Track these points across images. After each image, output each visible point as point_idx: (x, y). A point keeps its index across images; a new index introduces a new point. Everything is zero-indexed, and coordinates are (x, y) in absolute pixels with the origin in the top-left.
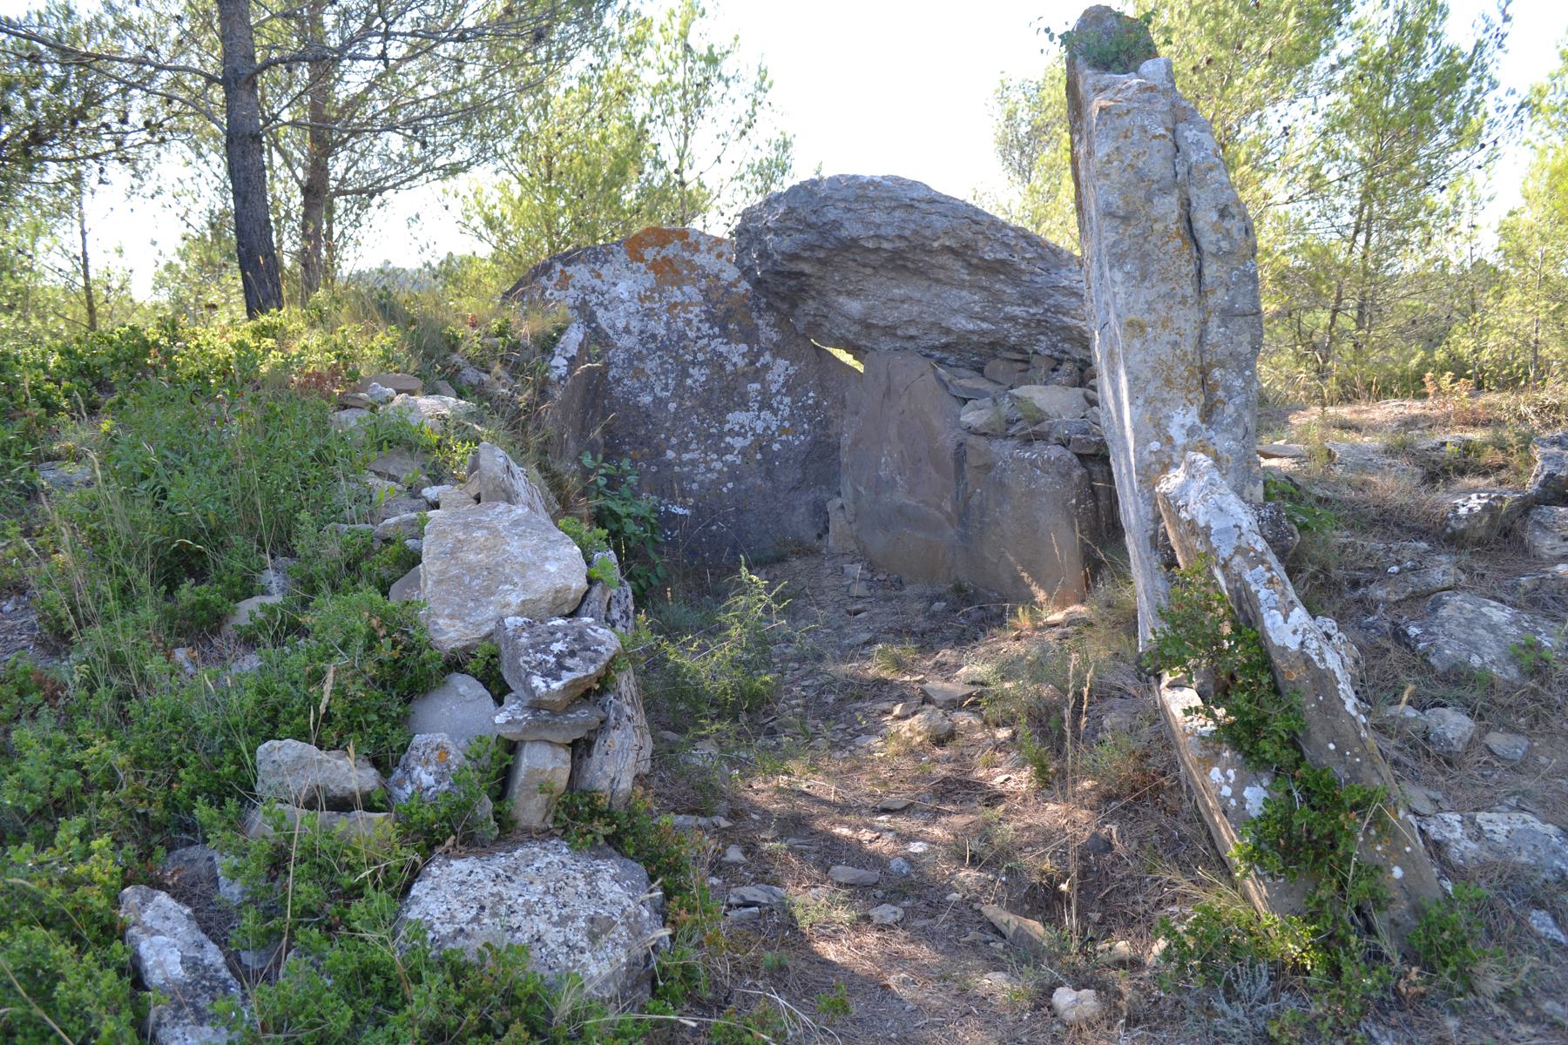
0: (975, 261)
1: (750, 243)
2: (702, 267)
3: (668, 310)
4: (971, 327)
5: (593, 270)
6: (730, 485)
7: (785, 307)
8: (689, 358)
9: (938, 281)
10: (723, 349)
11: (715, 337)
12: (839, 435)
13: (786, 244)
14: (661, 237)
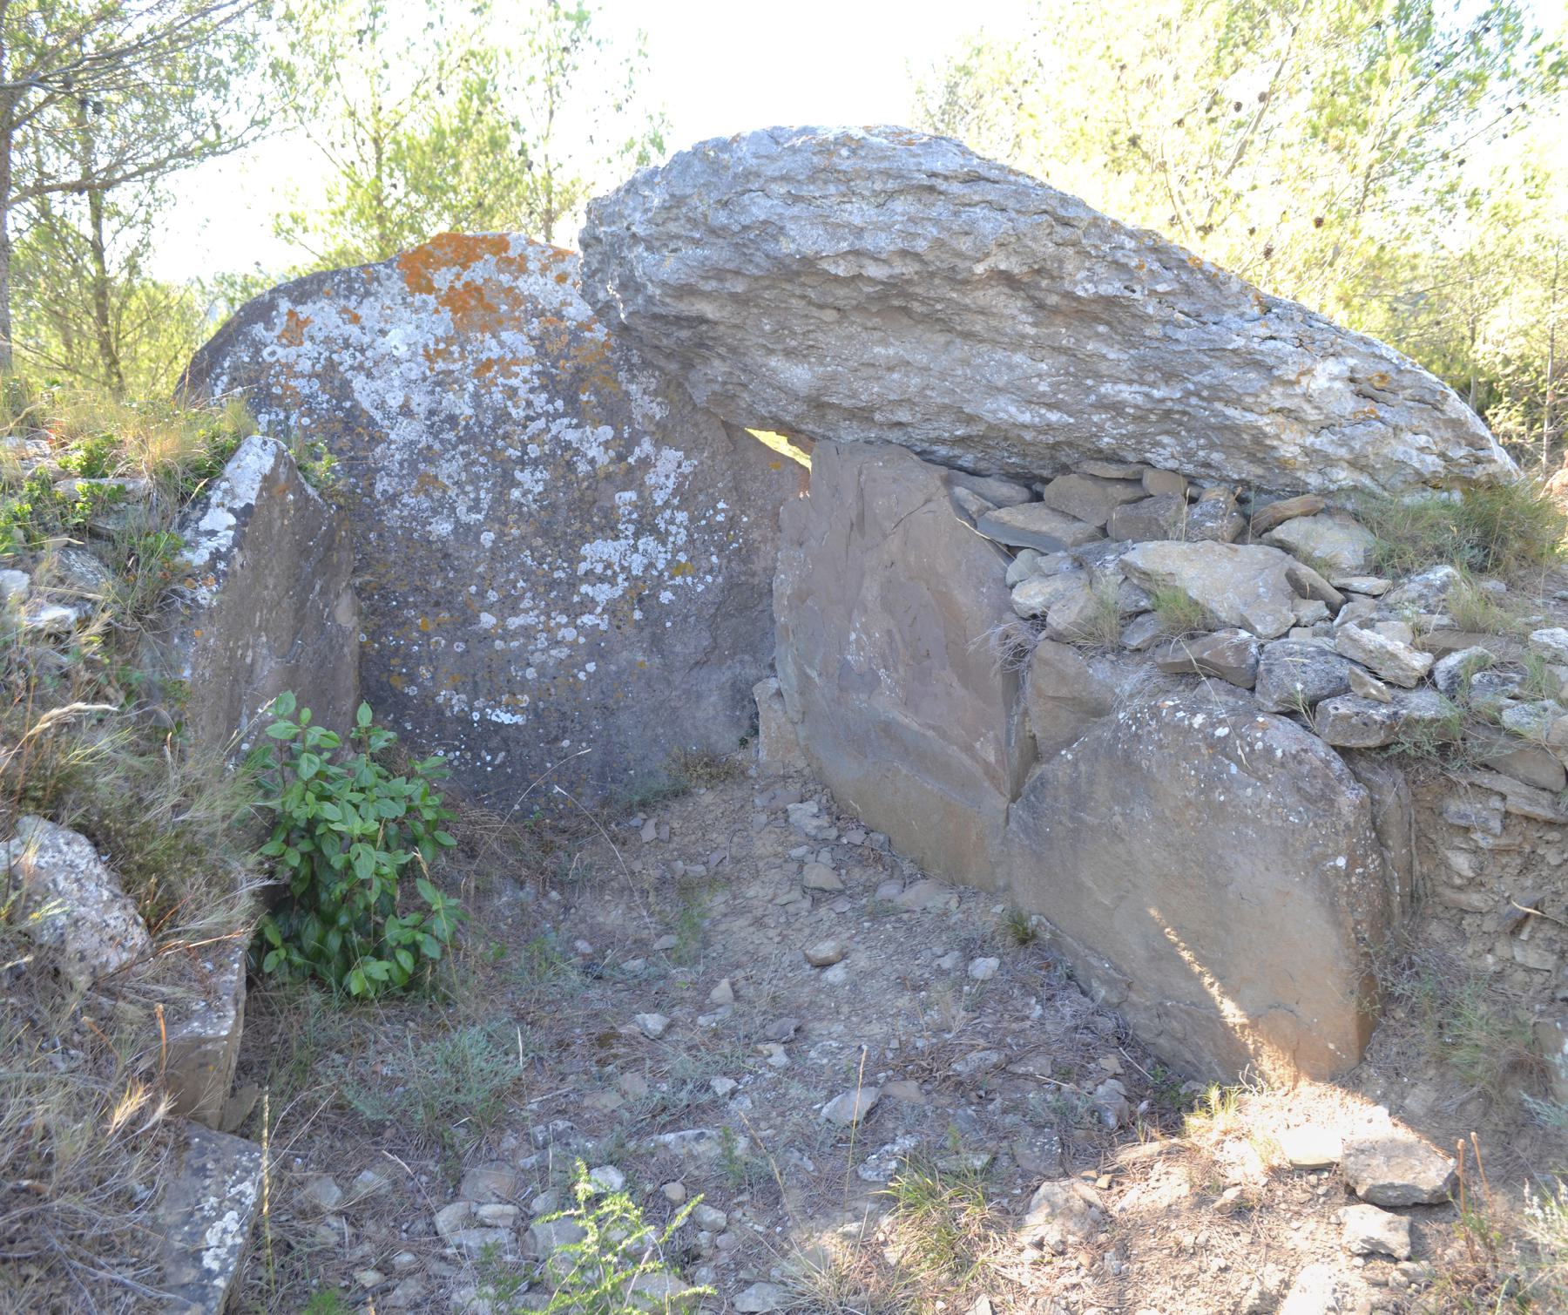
0: (1053, 300)
1: (605, 260)
2: (533, 299)
3: (478, 374)
4: (1026, 418)
5: (345, 310)
6: (591, 667)
7: (673, 367)
8: (514, 453)
9: (968, 335)
10: (571, 435)
11: (557, 415)
12: (771, 571)
13: (668, 267)
14: (461, 249)
